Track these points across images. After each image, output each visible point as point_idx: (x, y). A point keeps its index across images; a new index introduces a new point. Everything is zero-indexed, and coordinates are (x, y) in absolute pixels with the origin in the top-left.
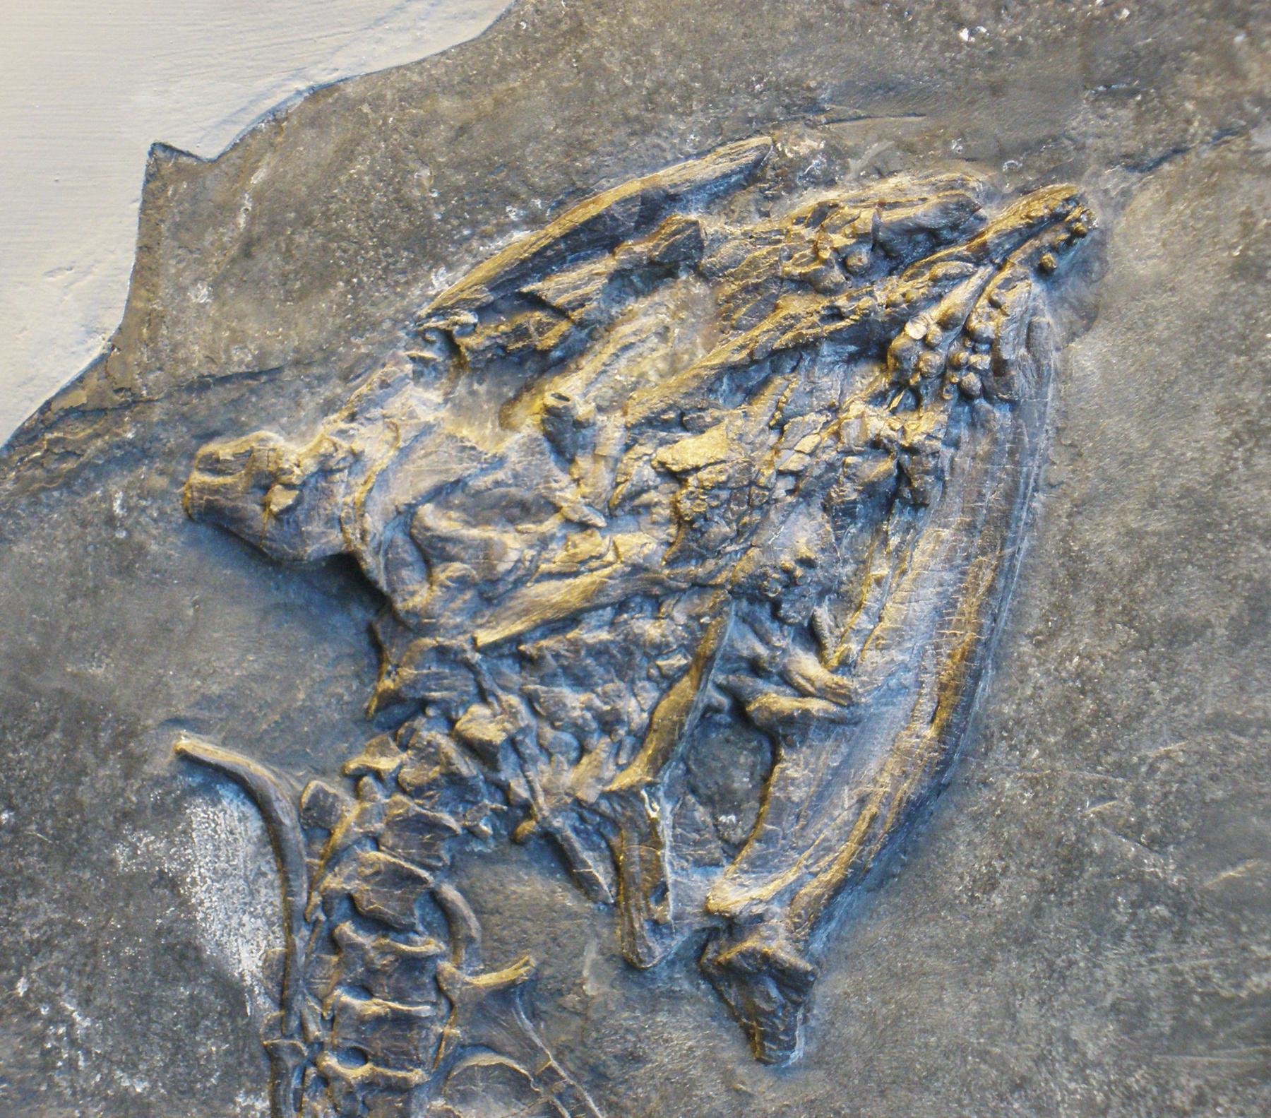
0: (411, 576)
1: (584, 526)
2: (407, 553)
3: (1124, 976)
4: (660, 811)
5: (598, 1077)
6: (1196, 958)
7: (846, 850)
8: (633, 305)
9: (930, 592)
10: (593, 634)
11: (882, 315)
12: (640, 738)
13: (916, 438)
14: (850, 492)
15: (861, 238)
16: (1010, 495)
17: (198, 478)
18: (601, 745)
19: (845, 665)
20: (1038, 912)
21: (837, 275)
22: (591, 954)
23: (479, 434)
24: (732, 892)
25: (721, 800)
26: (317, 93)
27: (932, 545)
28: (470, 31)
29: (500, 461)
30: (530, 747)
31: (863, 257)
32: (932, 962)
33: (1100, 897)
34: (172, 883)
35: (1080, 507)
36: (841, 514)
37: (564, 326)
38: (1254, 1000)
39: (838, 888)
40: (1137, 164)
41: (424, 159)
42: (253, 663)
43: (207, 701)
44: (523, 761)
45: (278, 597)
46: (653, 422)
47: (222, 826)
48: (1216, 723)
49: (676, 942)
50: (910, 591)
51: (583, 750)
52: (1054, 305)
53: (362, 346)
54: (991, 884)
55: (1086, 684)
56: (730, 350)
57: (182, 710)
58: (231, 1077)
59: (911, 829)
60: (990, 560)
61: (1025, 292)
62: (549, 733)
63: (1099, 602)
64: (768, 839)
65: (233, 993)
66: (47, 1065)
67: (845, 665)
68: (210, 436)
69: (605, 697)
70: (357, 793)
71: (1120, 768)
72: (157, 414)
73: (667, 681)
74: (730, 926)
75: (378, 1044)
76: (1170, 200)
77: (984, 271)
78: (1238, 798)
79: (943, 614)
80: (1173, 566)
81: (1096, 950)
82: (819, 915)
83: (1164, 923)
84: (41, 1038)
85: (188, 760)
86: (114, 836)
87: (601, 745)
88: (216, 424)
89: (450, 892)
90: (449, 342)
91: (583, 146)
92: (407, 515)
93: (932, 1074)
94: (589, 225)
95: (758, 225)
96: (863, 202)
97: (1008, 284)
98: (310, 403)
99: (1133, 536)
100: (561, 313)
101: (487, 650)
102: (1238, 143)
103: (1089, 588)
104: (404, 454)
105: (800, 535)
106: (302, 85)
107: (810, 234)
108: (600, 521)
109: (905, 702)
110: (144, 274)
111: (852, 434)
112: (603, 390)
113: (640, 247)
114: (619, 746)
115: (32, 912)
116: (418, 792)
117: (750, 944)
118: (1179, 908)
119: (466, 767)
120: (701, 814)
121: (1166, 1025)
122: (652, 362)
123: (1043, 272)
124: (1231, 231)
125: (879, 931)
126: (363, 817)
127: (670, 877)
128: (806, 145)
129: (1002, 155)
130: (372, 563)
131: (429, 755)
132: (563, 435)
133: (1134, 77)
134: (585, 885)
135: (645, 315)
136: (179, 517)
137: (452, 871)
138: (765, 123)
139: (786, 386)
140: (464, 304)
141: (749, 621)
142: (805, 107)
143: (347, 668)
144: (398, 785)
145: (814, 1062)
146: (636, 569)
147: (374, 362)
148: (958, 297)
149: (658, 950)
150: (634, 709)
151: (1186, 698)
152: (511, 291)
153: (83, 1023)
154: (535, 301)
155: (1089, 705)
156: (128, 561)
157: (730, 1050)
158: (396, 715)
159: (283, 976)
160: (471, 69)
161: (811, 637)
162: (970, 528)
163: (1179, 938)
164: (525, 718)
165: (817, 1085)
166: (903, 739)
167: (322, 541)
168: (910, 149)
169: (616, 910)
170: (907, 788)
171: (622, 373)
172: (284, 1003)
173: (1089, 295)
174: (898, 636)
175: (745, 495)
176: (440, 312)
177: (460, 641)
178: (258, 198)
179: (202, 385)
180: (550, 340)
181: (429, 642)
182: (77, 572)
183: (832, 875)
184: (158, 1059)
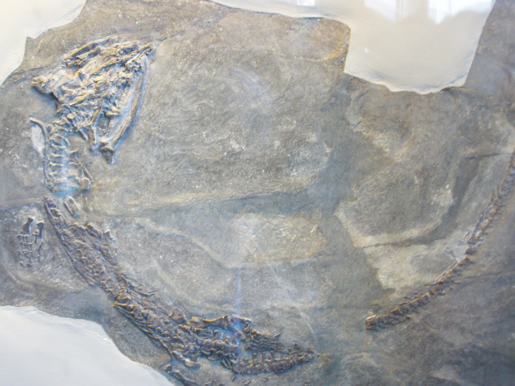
0: (61, 96)
1: (84, 89)
2: (60, 93)
3: (157, 152)
4: (94, 128)
5: (86, 166)
6: (167, 149)
7: (119, 134)
8: (92, 59)
9: (131, 98)
10: (85, 104)
11: (124, 60)
12: (92, 118)
13: (128, 77)
14: (120, 84)
15: (122, 49)
16: (142, 85)
17: (33, 82)
18: (86, 119)
19: (119, 108)
20: (145, 143)
21: (118, 55)
22: (85, 149)
23: (70, 76)
24: (104, 140)
25: (103, 127)
26: (49, 30)
27: (131, 92)
28: (70, 22)
29: (73, 80)
30: (77, 119)
31: (122, 52)
32: (131, 150)
33: (154, 141)
34: (29, 138)
35: (152, 87)
36: (119, 87)
37: (82, 62)
38: (174, 155)
39: (118, 139)
40: (160, 40)
41: (63, 39)
42: (40, 108)
43: (34, 113)
44: (76, 122)
45: (43, 99)
46: (93, 75)
47: (36, 131)
48: (169, 117)
49: (97, 147)
50: (128, 97)
51: (84, 120)
52: (149, 59)
53: (55, 64)
54: (139, 139)
55: (152, 111)
56: (104, 65)
57: (31, 114)
58: (38, 165)
59: (128, 130)
60: (139, 94)
61: (145, 57)
62: (79, 118)
63: (154, 100)
64: (109, 132)
65: (38, 154)
66: (13, 163)
67: (119, 108)
68: (34, 77)
69: (87, 113)
70: (54, 126)
71: (156, 123)
72: (27, 74)
73: (95, 110)
74: (103, 144)
75: (57, 161)
76: (165, 45)
77: (139, 54)
78: (173, 127)
79: (133, 101)
80: (164, 95)
81: (153, 148)
82: (116, 143)
83: (162, 145)
84: (12, 159)
85: (32, 122)
86: (22, 132)
87: (86, 119)
88: (35, 75)
89: (67, 140)
90: (66, 64)
91: (84, 37)
92: (60, 87)
93: (131, 165)
94: (85, 48)
95: (108, 48)
96: (122, 45)
97: (142, 56)
98: (48, 72)
99: (159, 91)
100: (81, 60)
101: (71, 106)
102: (174, 38)
103: (153, 98)
104: (60, 79)
105: (113, 90)
106: (47, 29)
107: (115, 49)
108: (86, 88)
109: (127, 114)
110: (26, 55)
111: (120, 76)
112: (87, 70)
113: (92, 51)
114: (88, 119)
115: (11, 142)
116: (62, 126)
117: (106, 147)
118: (164, 142)
119: (68, 122)
120: (100, 129)
121: (163, 158)
122: (94, 66)
123: (147, 55)
124: (173, 49)
125: (124, 145)
126: (55, 129)
127: (95, 137)
128: (115, 37)
129: (142, 39)
130: (55, 94)
131: (64, 121)
132: (81, 77)
133: (160, 28)
134: (84, 139)
135: (93, 60)
136: (30, 88)
137: (67, 137)
138: (110, 34)
139: (111, 70)
140: (68, 59)
141: (106, 102)
142: (115, 32)
143: (53, 109)
144: (59, 125)
145: (115, 163)
146: (90, 95)
147: (56, 67)
148: (135, 58)
149: (94, 148)
150: (91, 114)
151: (165, 113)
152: (75, 57)
153: (18, 157)
154: (78, 58)
155: (152, 114)
156: (23, 94)
157: (104, 162)
158: (59, 115)
159: (45, 152)
160: (70, 27)
161: (115, 104)
162: (136, 89)
163: (164, 146)
164: (76, 115)
165: (116, 167)
166: (127, 119)
167: (48, 91)
168: (129, 38)
169: (89, 142)
170: (127, 125)
171: (89, 68)
172: (45, 155)
173: (153, 58)
174: (126, 104)
175: (105, 85)
176: (65, 60)
177: (67, 105)
178: (41, 44)
179: (33, 70)
180: (79, 64)
181: (63, 105)
182: (17, 95)
183: (117, 137)
184: (28, 163)
